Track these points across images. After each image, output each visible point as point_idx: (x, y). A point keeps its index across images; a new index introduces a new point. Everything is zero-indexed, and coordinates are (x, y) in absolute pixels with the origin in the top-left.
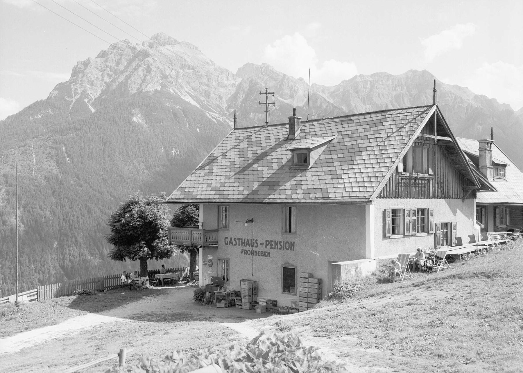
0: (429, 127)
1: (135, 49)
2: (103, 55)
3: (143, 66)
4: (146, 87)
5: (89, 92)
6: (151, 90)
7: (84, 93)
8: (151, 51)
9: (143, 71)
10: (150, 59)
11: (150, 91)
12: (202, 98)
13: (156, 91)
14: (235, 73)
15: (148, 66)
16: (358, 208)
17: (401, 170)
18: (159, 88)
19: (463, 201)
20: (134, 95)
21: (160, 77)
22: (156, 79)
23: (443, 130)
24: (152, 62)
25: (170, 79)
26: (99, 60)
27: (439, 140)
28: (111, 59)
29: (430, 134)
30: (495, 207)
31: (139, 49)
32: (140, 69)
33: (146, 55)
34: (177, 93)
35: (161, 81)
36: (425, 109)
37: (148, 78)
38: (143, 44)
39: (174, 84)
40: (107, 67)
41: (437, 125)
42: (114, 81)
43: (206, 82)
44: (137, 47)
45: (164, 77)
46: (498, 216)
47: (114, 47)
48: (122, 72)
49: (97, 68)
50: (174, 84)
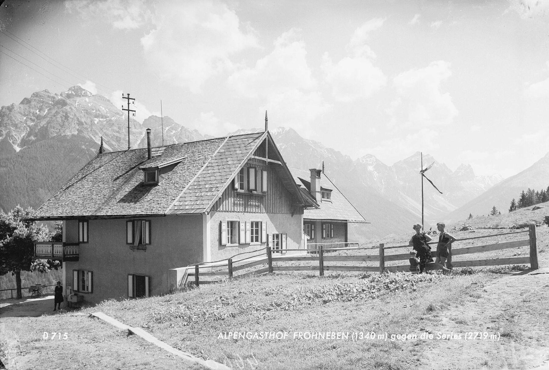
0: (261, 151)
1: (54, 98)
2: (26, 101)
3: (61, 113)
4: (64, 132)
5: (14, 133)
6: (69, 134)
7: (8, 135)
8: (68, 101)
9: (61, 117)
10: (67, 108)
11: (68, 135)
12: (114, 143)
13: (73, 135)
14: (141, 123)
15: (66, 114)
16: (195, 221)
17: (237, 186)
18: (76, 133)
19: (292, 216)
20: (53, 138)
21: (77, 123)
22: (73, 126)
23: (274, 153)
24: (69, 110)
25: (85, 126)
26: (22, 106)
27: (270, 163)
28: (33, 106)
29: (263, 157)
30: (324, 223)
31: (57, 99)
32: (59, 116)
33: (64, 103)
34: (91, 138)
35: (78, 127)
36: (257, 136)
37: (66, 123)
38: (61, 95)
39: (89, 130)
40: (30, 112)
41: (268, 148)
42: (36, 125)
43: (117, 130)
44: (55, 96)
45: (80, 123)
46: (324, 231)
47: (36, 95)
48: (45, 117)
49: (21, 113)
50: (89, 130)
